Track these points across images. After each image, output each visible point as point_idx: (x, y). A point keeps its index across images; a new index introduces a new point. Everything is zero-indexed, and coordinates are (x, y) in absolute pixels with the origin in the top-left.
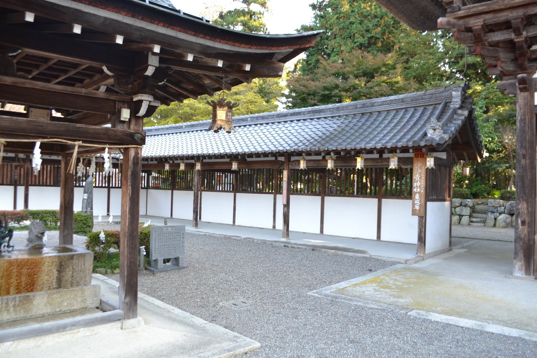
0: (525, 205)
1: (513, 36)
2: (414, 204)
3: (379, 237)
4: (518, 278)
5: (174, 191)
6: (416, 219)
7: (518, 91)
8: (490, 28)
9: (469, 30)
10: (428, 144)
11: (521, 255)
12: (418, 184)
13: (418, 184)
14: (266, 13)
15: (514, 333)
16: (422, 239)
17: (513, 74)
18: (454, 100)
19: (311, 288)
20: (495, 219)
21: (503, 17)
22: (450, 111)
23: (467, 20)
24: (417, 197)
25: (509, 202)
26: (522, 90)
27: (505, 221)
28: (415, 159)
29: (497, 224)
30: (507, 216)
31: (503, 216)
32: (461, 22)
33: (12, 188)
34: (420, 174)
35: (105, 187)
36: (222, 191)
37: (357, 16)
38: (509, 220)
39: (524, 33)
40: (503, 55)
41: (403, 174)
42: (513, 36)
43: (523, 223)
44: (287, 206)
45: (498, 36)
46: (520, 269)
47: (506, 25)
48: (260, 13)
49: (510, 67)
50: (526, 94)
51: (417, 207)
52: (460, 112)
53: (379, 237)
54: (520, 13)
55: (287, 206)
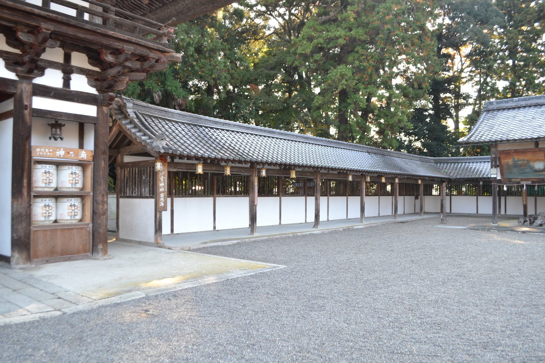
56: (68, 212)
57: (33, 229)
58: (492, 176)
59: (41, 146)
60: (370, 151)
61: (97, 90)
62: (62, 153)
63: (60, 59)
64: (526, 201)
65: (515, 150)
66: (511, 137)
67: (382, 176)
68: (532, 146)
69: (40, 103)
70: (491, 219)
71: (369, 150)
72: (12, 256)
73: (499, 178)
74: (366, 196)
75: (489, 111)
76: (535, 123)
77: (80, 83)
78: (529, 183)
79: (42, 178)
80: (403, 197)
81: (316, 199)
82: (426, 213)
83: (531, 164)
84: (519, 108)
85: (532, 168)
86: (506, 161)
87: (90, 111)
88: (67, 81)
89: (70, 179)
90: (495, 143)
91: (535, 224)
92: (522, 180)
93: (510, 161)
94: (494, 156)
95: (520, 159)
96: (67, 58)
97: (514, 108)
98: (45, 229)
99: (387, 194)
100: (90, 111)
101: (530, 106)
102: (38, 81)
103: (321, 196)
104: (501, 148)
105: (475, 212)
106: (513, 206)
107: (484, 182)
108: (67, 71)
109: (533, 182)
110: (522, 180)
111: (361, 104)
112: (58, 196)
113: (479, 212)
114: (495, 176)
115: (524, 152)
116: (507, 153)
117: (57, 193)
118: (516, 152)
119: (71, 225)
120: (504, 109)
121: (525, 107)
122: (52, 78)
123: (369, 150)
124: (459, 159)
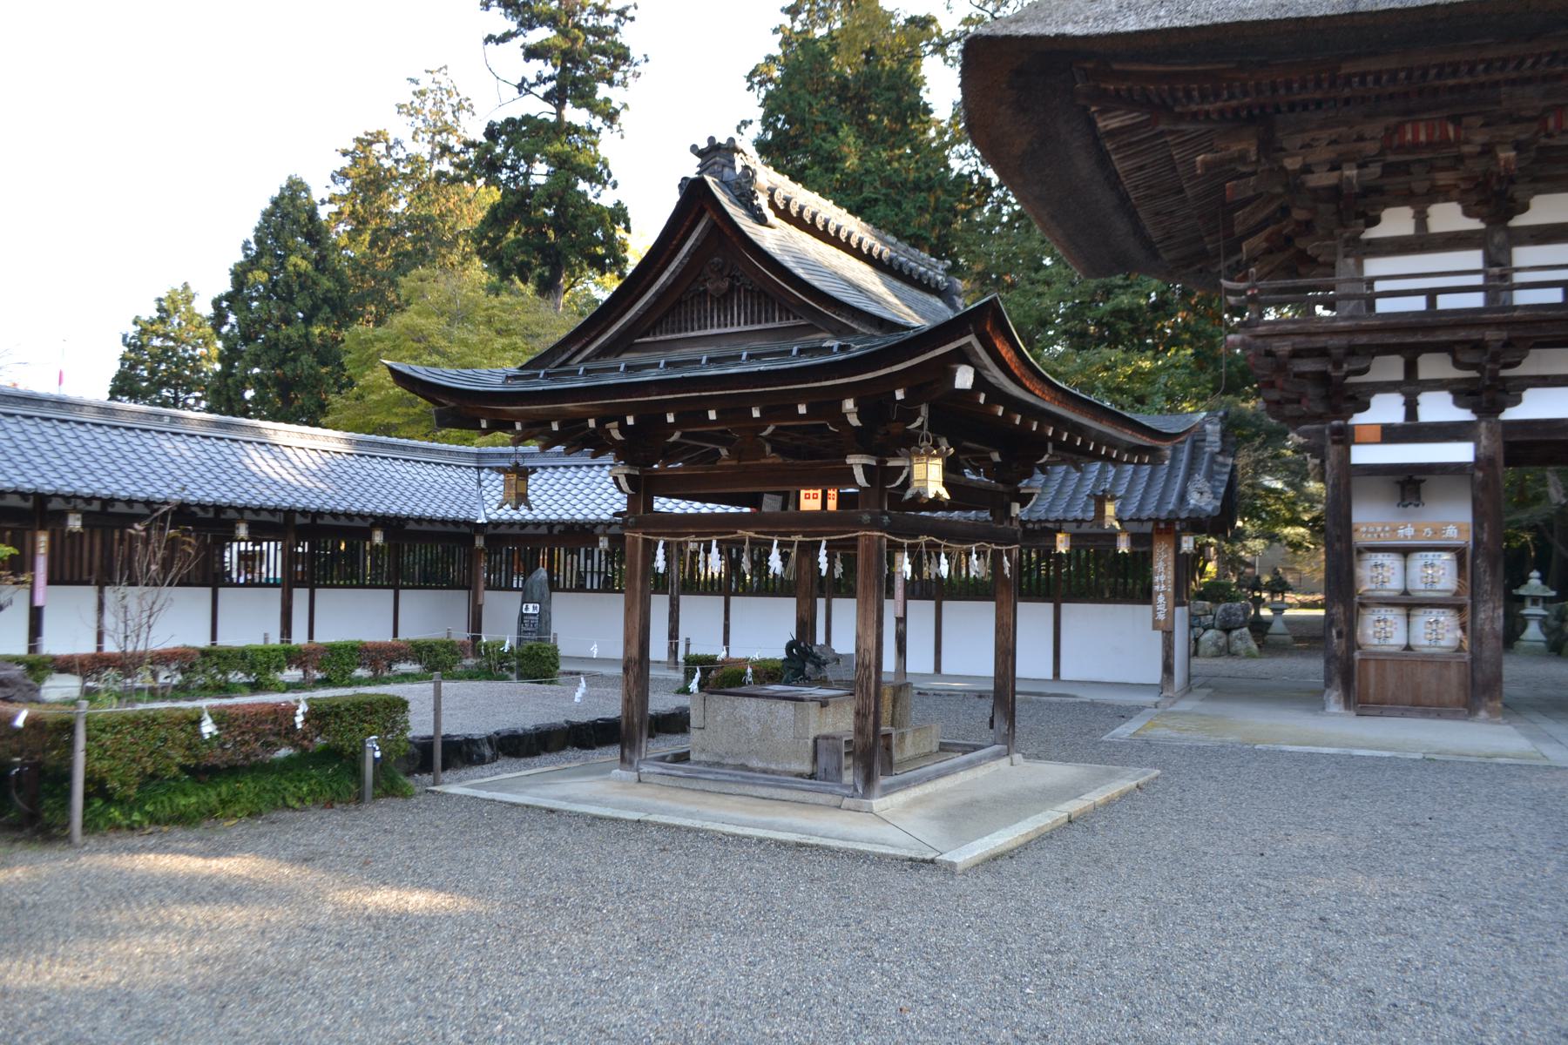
0: (1341, 609)
1: (1330, 368)
2: (1155, 612)
3: (1057, 673)
4: (1335, 714)
5: (221, 590)
6: (1159, 634)
7: (1329, 443)
8: (1296, 354)
9: (1269, 353)
10: (1194, 515)
11: (1337, 681)
12: (1162, 578)
13: (1162, 578)
14: (605, 130)
15: (1386, 754)
16: (1168, 668)
17: (1318, 418)
18: (1209, 438)
19: (1105, 731)
20: (1196, 640)
21: (1320, 342)
22: (1206, 457)
23: (1269, 340)
24: (1161, 599)
25: (1222, 606)
26: (1334, 442)
27: (1215, 644)
28: (1155, 537)
29: (1201, 651)
30: (1219, 633)
31: (1210, 634)
32: (1259, 342)
33: (207, 591)
34: (1165, 561)
35: (518, 589)
36: (246, 585)
37: (878, 184)
38: (1222, 642)
39: (1345, 366)
40: (1312, 391)
41: (1140, 563)
42: (1330, 368)
43: (1340, 635)
44: (902, 621)
45: (1307, 366)
46: (1337, 702)
47: (1323, 353)
48: (591, 131)
49: (1320, 408)
50: (1340, 447)
51: (1161, 617)
52: (1220, 459)
53: (1057, 673)
54: (1343, 341)
55: (902, 621)
56: (1439, 632)
57: (1357, 655)
59: (1372, 519)
61: (1474, 412)
62: (1410, 531)
63: (1398, 375)
69: (1362, 455)
72: (1265, 642)
74: (51, 581)
77: (1437, 408)
79: (1380, 575)
87: (1461, 452)
88: (1411, 408)
89: (1440, 574)
96: (1411, 368)
98: (1382, 659)
100: (1461, 452)
102: (1519, 221)
108: (1411, 388)
112: (1409, 604)
117: (1405, 600)
119: (1433, 655)
122: (1387, 409)
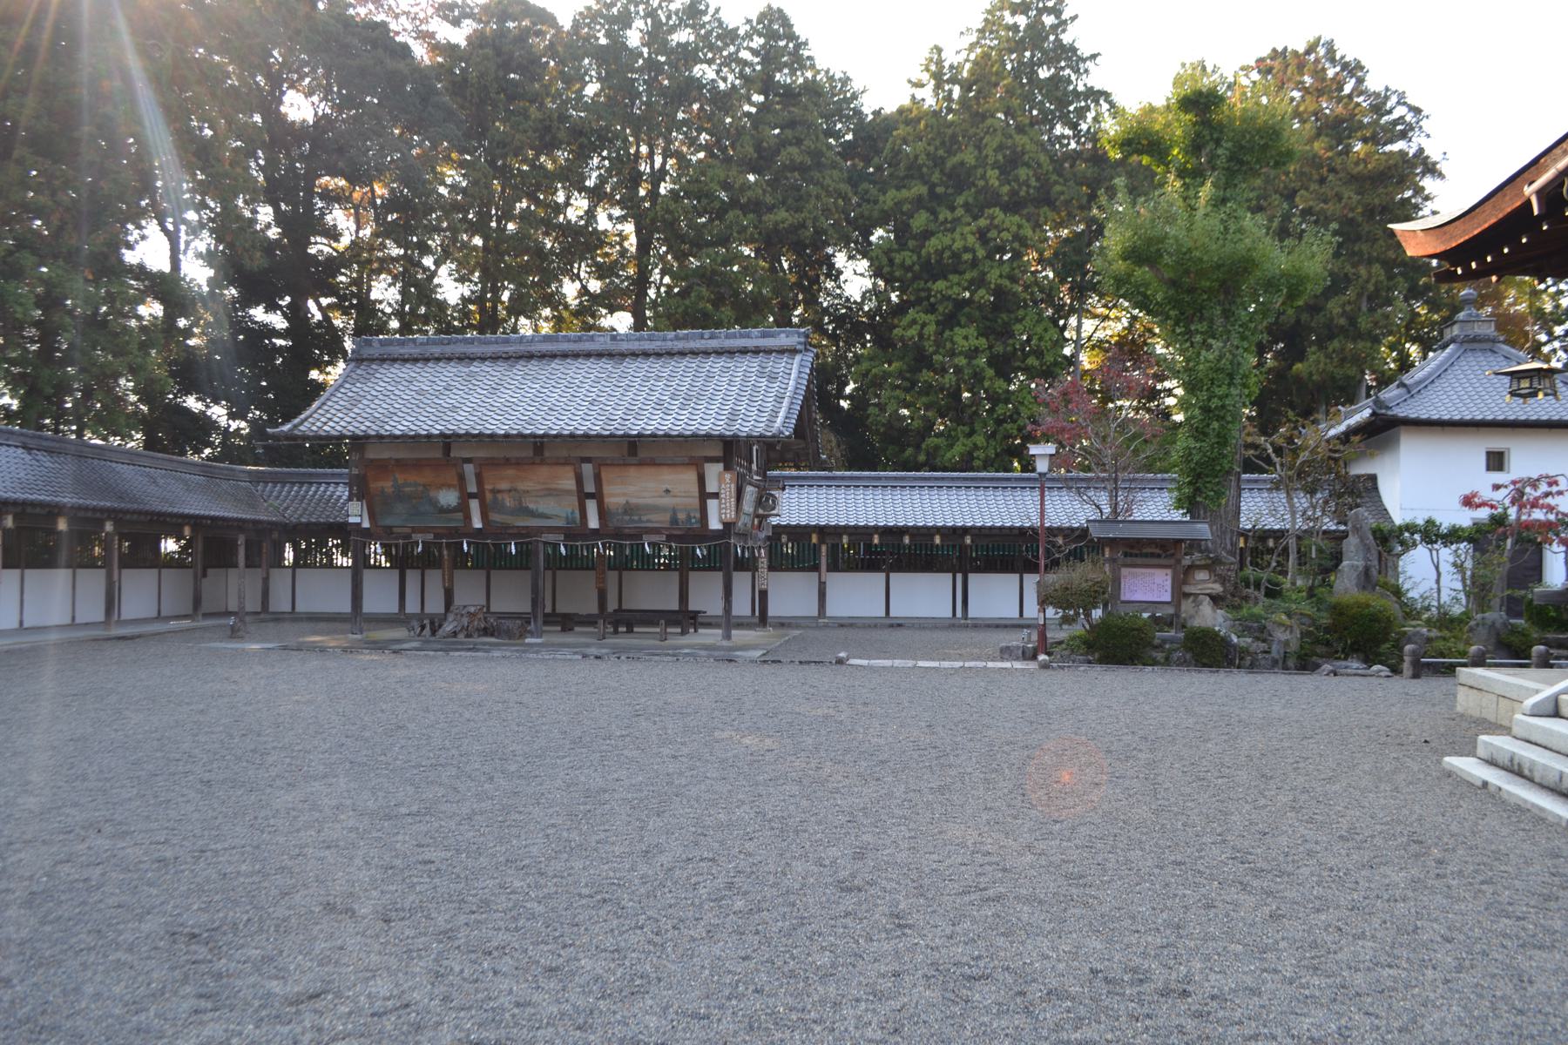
58: (352, 520)
60: (32, 443)
64: (451, 580)
65: (397, 460)
66: (387, 429)
67: (59, 514)
68: (438, 454)
70: (348, 626)
71: (28, 441)
73: (366, 524)
74: (771, 568)
75: (363, 360)
76: (447, 401)
78: (430, 537)
80: (17, 572)
81: (109, 576)
82: (206, 615)
83: (432, 494)
84: (427, 360)
85: (434, 503)
86: (380, 484)
90: (360, 442)
91: (440, 632)
92: (414, 530)
93: (387, 485)
94: (355, 471)
95: (410, 481)
97: (416, 360)
99: (91, 564)
101: (450, 359)
103: (1540, 579)
104: (372, 454)
105: (395, 609)
106: (578, 595)
107: (912, 537)
109: (437, 536)
110: (414, 530)
111: (19, 309)
113: (298, 609)
114: (357, 520)
115: (418, 465)
116: (382, 467)
118: (401, 464)
120: (394, 360)
121: (438, 360)
123: (28, 441)
124: (311, 475)
